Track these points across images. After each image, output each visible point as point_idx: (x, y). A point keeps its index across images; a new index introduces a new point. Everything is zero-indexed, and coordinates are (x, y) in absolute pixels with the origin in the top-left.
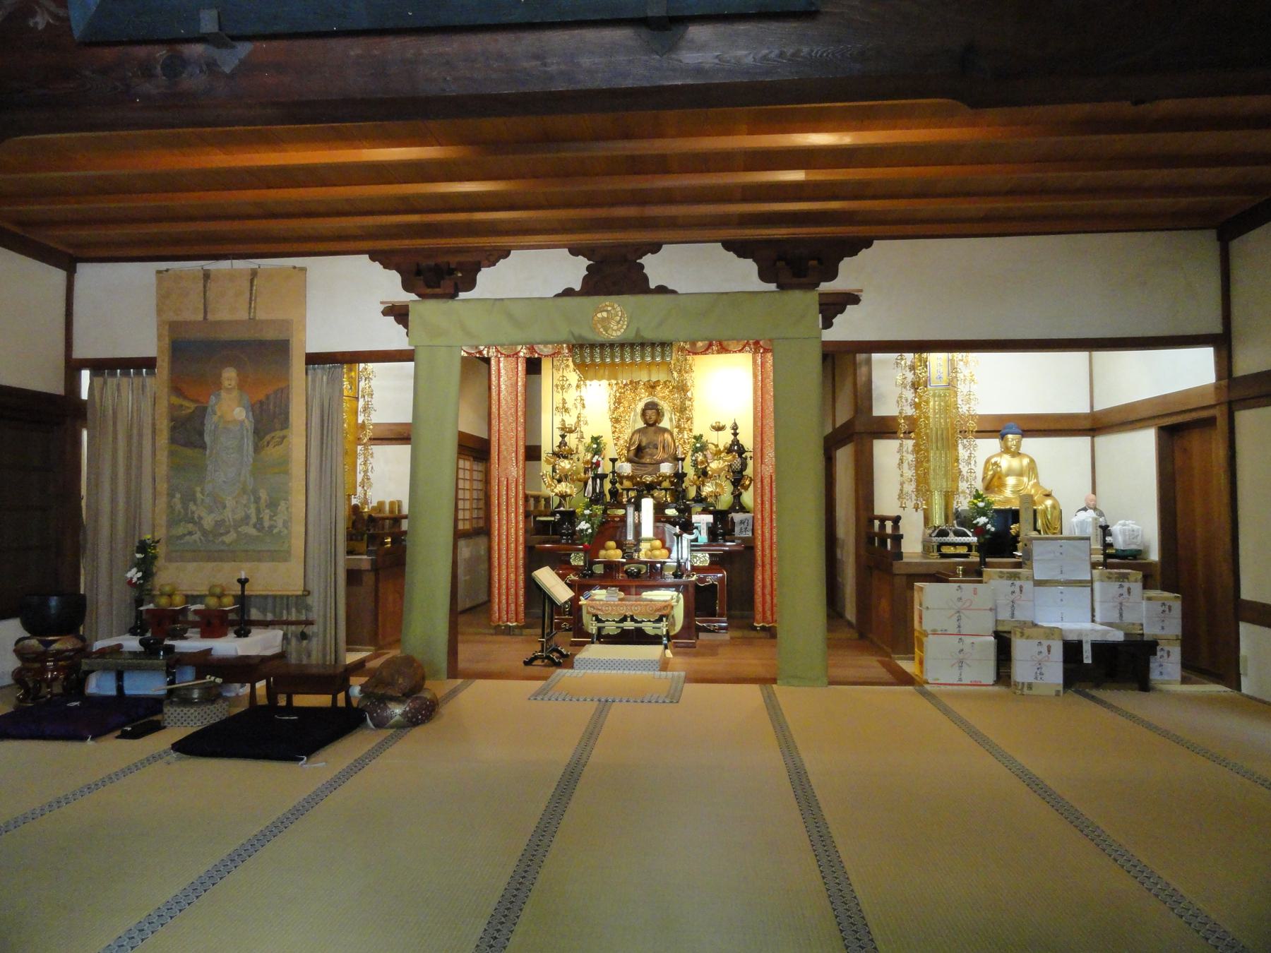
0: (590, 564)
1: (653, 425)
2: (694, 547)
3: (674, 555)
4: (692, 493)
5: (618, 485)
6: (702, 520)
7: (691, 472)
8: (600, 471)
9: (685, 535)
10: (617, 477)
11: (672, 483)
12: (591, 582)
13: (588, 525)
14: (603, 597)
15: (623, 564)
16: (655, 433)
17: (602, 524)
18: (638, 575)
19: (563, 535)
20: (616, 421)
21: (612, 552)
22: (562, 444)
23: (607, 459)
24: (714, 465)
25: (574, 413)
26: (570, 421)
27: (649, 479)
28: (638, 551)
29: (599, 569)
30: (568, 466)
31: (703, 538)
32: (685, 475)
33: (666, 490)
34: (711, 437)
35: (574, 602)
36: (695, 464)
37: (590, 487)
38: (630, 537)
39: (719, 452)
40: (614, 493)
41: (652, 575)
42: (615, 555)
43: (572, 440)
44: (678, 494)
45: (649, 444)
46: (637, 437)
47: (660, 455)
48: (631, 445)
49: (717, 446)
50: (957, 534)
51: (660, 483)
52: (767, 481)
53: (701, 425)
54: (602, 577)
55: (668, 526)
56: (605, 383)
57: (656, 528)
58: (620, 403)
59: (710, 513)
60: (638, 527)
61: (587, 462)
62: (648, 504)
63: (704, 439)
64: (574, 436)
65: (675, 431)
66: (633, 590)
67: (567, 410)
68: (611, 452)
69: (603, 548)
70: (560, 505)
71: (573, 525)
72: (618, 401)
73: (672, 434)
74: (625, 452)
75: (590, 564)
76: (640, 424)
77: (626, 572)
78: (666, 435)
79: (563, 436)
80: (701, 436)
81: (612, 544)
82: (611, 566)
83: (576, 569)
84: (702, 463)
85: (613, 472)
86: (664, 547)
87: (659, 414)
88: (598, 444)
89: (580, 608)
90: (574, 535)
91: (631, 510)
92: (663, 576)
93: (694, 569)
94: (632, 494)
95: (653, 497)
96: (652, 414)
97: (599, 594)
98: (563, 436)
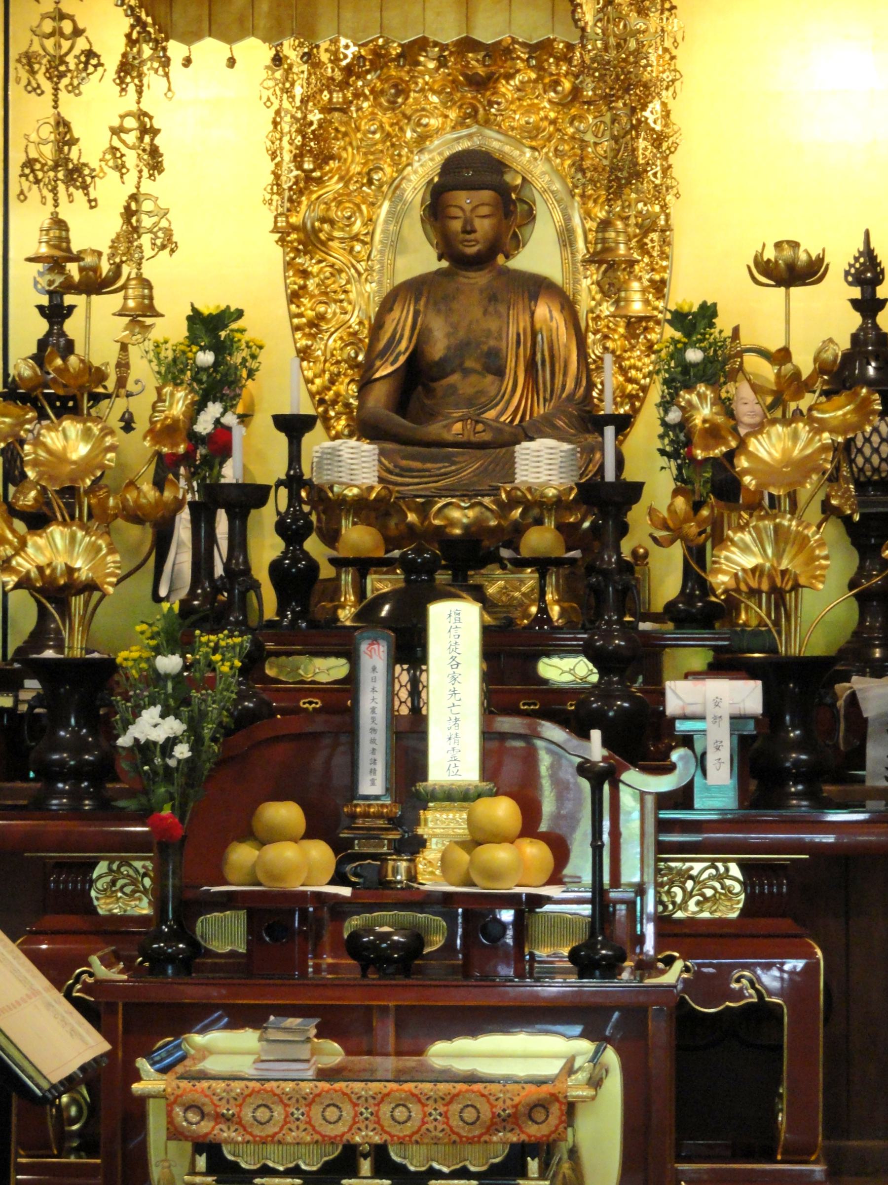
0: (183, 907)
1: (482, 260)
2: (676, 829)
3: (580, 865)
4: (666, 581)
5: (313, 545)
6: (711, 703)
7: (659, 485)
8: (230, 473)
9: (632, 776)
10: (312, 507)
11: (568, 532)
12: (191, 992)
13: (173, 726)
14: (245, 1066)
15: (338, 909)
16: (492, 297)
17: (241, 721)
18: (409, 957)
19: (50, 774)
20: (304, 242)
21: (286, 854)
22: (55, 344)
23: (263, 421)
24: (771, 447)
25: (112, 191)
26: (93, 230)
27: (461, 516)
28: (414, 845)
29: (224, 934)
30: (80, 450)
31: (718, 788)
32: (634, 491)
33: (543, 565)
34: (760, 317)
35: (104, 1082)
36: (679, 440)
37: (181, 557)
38: (373, 781)
39: (796, 384)
40: (295, 578)
41: (470, 961)
42: (301, 862)
43: (97, 326)
44: (600, 585)
45: (461, 349)
46: (402, 318)
47: (512, 401)
48: (374, 356)
49: (783, 356)
51: (513, 535)
53: (708, 258)
54: (237, 967)
55: (553, 732)
56: (254, 52)
57: (490, 737)
58: (323, 158)
59: (749, 671)
60: (409, 736)
61: (165, 432)
62: (455, 629)
63: (723, 324)
64: (105, 305)
65: (586, 289)
66: (387, 1031)
67: (77, 176)
68: (280, 383)
69: (249, 833)
70: (40, 636)
71: (106, 728)
72: (315, 151)
73: (568, 306)
74: (348, 389)
75: (183, 907)
76: (422, 258)
77: (354, 946)
78: (546, 312)
79: (55, 313)
80: (708, 312)
81: (286, 813)
82: (277, 917)
83: (116, 933)
84: (713, 433)
85: (294, 481)
86: (529, 827)
87: (513, 210)
88: (221, 348)
89: (137, 1108)
90: (103, 769)
91: (375, 657)
92: (527, 967)
93: (672, 931)
94: (379, 584)
95: (478, 594)
96: (476, 209)
97: (228, 1051)
98: (55, 313)
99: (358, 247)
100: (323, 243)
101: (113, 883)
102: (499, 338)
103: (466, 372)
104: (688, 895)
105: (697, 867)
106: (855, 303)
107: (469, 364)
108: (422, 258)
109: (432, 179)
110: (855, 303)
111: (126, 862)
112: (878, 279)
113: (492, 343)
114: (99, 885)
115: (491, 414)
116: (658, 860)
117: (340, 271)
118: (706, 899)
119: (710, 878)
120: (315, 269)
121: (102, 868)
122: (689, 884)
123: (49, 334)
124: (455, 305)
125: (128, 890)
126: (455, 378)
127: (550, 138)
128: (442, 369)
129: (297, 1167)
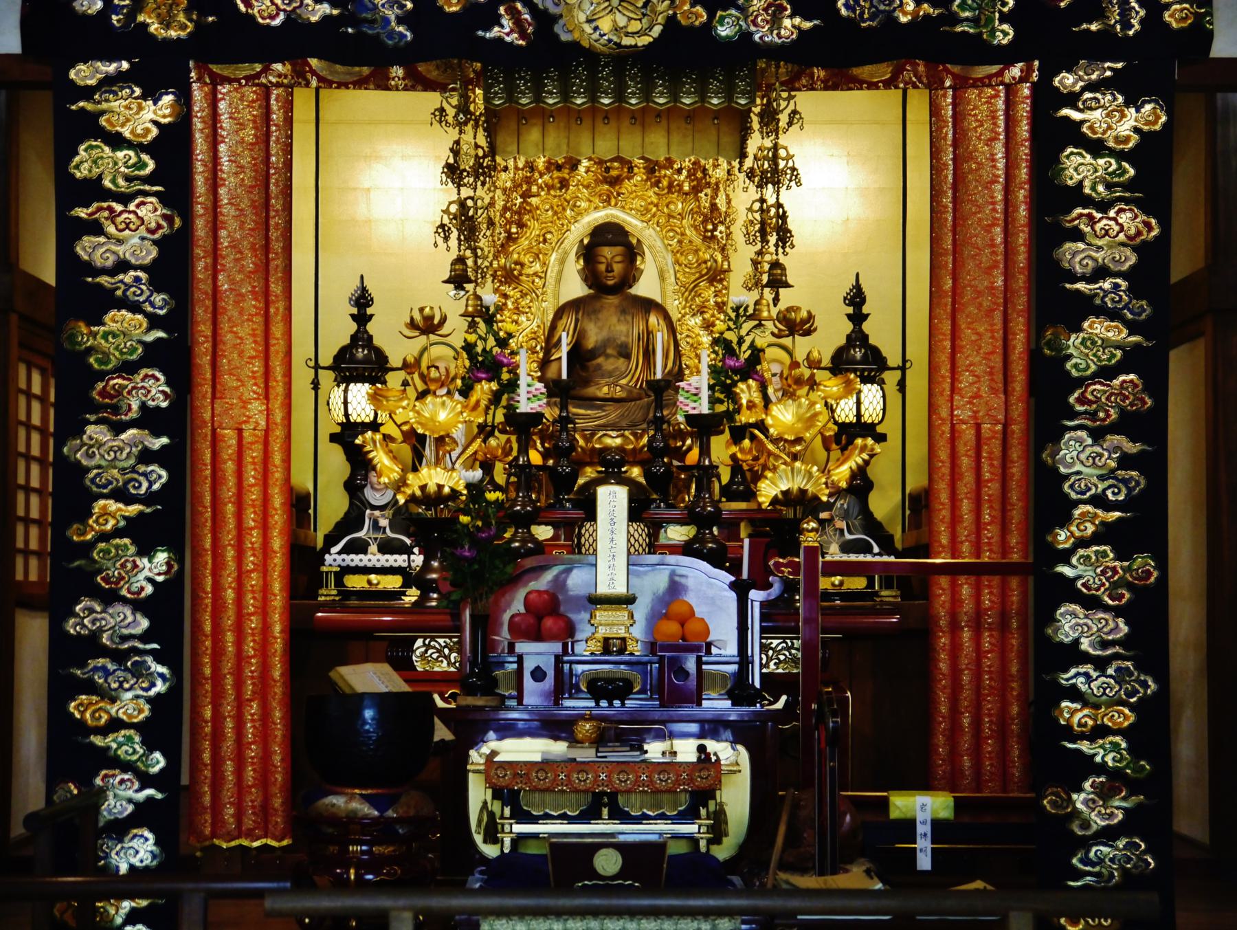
50: (387, 547)
52: (968, 433)
76: (575, 288)
99: (537, 280)
100: (517, 278)
101: (426, 652)
102: (627, 336)
103: (608, 356)
104: (769, 659)
105: (775, 642)
106: (849, 316)
107: (609, 351)
108: (575, 288)
109: (582, 241)
110: (849, 316)
111: (433, 638)
112: (863, 301)
113: (623, 339)
114: (418, 653)
115: (624, 382)
116: (761, 638)
117: (526, 294)
118: (780, 662)
119: (783, 649)
120: (512, 293)
121: (419, 642)
122: (771, 652)
123: (358, 331)
124: (600, 316)
125: (435, 656)
126: (600, 360)
127: (654, 216)
128: (593, 354)
129: (565, 814)
